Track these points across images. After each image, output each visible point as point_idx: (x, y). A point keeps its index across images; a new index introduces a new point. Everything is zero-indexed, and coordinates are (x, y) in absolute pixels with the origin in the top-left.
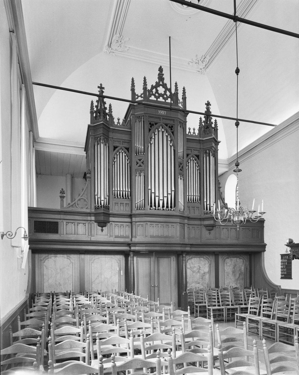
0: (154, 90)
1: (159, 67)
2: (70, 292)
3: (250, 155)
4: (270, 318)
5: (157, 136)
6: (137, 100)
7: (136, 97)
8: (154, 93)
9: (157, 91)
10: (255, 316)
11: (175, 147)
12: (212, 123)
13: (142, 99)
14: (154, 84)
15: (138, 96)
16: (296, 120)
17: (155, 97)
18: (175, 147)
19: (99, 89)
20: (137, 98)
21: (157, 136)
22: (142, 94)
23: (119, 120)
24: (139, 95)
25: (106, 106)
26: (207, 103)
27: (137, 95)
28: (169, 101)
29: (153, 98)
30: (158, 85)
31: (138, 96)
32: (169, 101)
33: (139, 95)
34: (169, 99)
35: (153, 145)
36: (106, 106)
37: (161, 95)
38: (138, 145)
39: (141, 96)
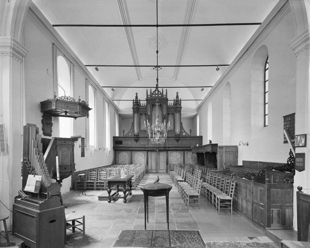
0: (154, 93)
9: (155, 93)
23: (143, 104)
28: (160, 95)
29: (154, 96)
32: (160, 95)
37: (156, 94)
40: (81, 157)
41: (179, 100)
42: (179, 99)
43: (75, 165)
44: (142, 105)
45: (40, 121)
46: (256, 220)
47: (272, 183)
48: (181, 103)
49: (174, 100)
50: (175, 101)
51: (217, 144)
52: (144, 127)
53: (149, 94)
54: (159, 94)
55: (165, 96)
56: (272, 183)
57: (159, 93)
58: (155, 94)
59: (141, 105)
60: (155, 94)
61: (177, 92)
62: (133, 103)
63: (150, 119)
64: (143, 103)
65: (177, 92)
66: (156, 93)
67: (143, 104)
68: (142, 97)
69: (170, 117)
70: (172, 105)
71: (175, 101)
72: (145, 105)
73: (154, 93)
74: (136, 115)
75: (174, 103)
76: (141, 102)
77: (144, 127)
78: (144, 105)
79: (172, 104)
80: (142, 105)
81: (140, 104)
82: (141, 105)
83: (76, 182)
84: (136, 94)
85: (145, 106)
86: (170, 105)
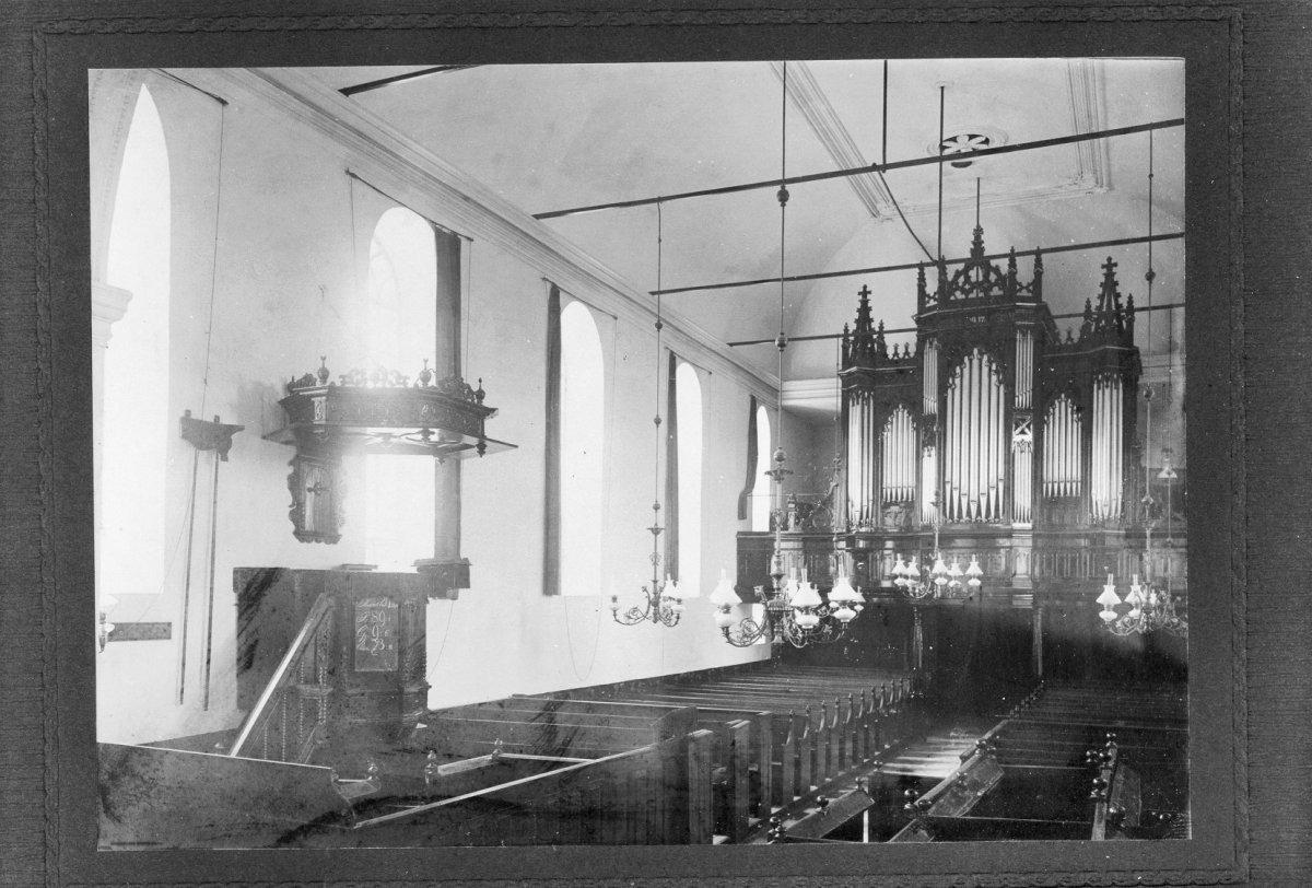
1: (182, 414)
4: (773, 760)
5: (966, 371)
6: (928, 305)
7: (1031, 288)
8: (960, 284)
9: (968, 278)
10: (771, 755)
11: (1009, 383)
15: (1022, 288)
17: (963, 291)
18: (1009, 383)
19: (1105, 271)
20: (1020, 290)
21: (966, 371)
22: (1029, 285)
23: (896, 348)
24: (1024, 284)
25: (1121, 301)
26: (1106, 263)
27: (1020, 284)
28: (996, 291)
29: (959, 295)
30: (969, 264)
31: (1022, 288)
32: (996, 291)
33: (1024, 284)
34: (996, 289)
35: (957, 392)
36: (1121, 301)
42: (1123, 301)
43: (430, 692)
44: (896, 354)
45: (285, 483)
49: (846, 335)
51: (467, 585)
52: (898, 476)
53: (932, 287)
54: (991, 286)
55: (1024, 293)
57: (993, 277)
58: (964, 283)
59: (890, 352)
60: (967, 287)
61: (865, 287)
62: (845, 348)
63: (931, 432)
64: (899, 342)
65: (865, 287)
66: (973, 279)
67: (896, 348)
69: (1062, 411)
70: (912, 355)
71: (852, 338)
73: (961, 279)
74: (855, 413)
75: (1085, 329)
77: (898, 476)
78: (907, 353)
80: (896, 354)
81: (883, 346)
82: (890, 357)
86: (901, 356)
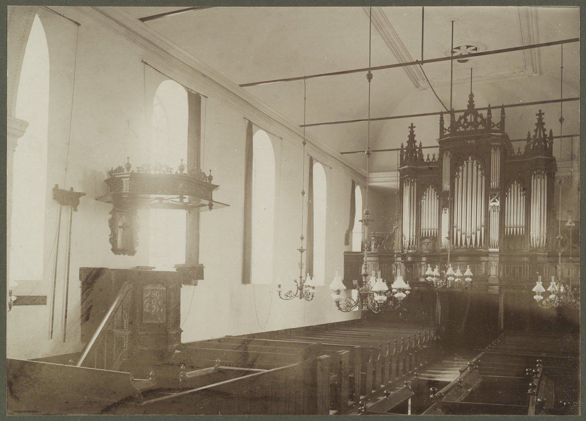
0: (463, 121)
2: (377, 280)
3: (359, 215)
7: (492, 125)
8: (462, 123)
9: (466, 120)
12: (481, 169)
13: (499, 129)
14: (414, 129)
15: (494, 125)
16: (71, 213)
19: (538, 117)
20: (493, 127)
22: (498, 124)
24: (496, 123)
27: (493, 124)
28: (481, 127)
29: (461, 129)
31: (494, 125)
33: (496, 123)
36: (416, 144)
37: (471, 124)
38: (446, 186)
39: (497, 125)
40: (203, 279)
41: (416, 147)
42: (547, 133)
46: (153, 400)
47: (409, 412)
48: (551, 144)
49: (402, 149)
50: (405, 151)
52: (429, 223)
53: (447, 125)
56: (409, 412)
57: (479, 120)
58: (464, 123)
61: (412, 124)
64: (430, 153)
65: (412, 124)
68: (429, 137)
70: (437, 160)
72: (437, 157)
73: (463, 121)
75: (527, 147)
76: (425, 152)
78: (434, 159)
79: (523, 151)
80: (428, 159)
81: (421, 155)
83: (411, 414)
84: (537, 115)
85: (435, 163)
86: (431, 160)
